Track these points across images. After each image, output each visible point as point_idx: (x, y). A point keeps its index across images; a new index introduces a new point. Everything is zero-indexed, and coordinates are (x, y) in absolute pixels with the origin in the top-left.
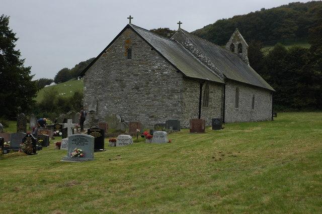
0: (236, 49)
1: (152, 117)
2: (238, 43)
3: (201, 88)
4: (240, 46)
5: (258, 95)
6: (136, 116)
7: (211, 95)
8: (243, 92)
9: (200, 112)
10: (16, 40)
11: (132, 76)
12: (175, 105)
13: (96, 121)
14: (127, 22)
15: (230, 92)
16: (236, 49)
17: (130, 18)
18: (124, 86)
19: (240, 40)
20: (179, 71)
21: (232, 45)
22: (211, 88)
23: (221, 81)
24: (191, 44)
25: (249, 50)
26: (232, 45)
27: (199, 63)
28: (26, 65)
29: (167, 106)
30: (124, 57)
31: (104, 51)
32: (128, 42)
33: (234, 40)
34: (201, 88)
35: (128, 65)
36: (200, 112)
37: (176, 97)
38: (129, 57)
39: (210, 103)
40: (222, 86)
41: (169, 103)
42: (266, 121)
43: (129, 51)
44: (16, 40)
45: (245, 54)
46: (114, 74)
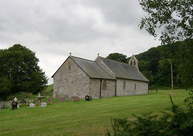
0: (133, 63)
1: (78, 94)
2: (134, 61)
3: (101, 82)
4: (135, 61)
5: (138, 84)
6: (72, 94)
7: (107, 85)
8: (128, 83)
9: (100, 92)
10: (39, 61)
11: (71, 77)
12: (87, 89)
13: (58, 96)
14: (69, 55)
15: (120, 83)
16: (133, 63)
17: (70, 53)
18: (68, 82)
19: (134, 59)
20: (88, 75)
21: (131, 62)
22: (107, 82)
23: (115, 78)
24: (102, 63)
25: (138, 64)
26: (131, 62)
27: (106, 71)
28: (43, 72)
29: (84, 90)
30: (68, 70)
31: (60, 67)
32: (69, 63)
33: (132, 60)
34: (101, 82)
35: (69, 73)
36: (100, 92)
37: (87, 86)
38: (70, 69)
39: (107, 88)
40: (115, 80)
41: (84, 88)
42: (144, 95)
43: (70, 67)
44: (39, 61)
45: (137, 66)
46: (64, 77)
